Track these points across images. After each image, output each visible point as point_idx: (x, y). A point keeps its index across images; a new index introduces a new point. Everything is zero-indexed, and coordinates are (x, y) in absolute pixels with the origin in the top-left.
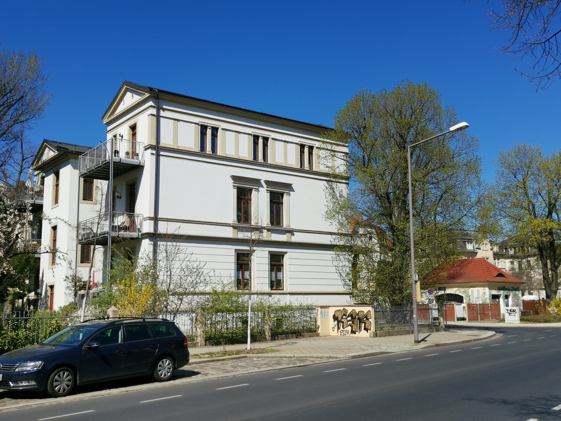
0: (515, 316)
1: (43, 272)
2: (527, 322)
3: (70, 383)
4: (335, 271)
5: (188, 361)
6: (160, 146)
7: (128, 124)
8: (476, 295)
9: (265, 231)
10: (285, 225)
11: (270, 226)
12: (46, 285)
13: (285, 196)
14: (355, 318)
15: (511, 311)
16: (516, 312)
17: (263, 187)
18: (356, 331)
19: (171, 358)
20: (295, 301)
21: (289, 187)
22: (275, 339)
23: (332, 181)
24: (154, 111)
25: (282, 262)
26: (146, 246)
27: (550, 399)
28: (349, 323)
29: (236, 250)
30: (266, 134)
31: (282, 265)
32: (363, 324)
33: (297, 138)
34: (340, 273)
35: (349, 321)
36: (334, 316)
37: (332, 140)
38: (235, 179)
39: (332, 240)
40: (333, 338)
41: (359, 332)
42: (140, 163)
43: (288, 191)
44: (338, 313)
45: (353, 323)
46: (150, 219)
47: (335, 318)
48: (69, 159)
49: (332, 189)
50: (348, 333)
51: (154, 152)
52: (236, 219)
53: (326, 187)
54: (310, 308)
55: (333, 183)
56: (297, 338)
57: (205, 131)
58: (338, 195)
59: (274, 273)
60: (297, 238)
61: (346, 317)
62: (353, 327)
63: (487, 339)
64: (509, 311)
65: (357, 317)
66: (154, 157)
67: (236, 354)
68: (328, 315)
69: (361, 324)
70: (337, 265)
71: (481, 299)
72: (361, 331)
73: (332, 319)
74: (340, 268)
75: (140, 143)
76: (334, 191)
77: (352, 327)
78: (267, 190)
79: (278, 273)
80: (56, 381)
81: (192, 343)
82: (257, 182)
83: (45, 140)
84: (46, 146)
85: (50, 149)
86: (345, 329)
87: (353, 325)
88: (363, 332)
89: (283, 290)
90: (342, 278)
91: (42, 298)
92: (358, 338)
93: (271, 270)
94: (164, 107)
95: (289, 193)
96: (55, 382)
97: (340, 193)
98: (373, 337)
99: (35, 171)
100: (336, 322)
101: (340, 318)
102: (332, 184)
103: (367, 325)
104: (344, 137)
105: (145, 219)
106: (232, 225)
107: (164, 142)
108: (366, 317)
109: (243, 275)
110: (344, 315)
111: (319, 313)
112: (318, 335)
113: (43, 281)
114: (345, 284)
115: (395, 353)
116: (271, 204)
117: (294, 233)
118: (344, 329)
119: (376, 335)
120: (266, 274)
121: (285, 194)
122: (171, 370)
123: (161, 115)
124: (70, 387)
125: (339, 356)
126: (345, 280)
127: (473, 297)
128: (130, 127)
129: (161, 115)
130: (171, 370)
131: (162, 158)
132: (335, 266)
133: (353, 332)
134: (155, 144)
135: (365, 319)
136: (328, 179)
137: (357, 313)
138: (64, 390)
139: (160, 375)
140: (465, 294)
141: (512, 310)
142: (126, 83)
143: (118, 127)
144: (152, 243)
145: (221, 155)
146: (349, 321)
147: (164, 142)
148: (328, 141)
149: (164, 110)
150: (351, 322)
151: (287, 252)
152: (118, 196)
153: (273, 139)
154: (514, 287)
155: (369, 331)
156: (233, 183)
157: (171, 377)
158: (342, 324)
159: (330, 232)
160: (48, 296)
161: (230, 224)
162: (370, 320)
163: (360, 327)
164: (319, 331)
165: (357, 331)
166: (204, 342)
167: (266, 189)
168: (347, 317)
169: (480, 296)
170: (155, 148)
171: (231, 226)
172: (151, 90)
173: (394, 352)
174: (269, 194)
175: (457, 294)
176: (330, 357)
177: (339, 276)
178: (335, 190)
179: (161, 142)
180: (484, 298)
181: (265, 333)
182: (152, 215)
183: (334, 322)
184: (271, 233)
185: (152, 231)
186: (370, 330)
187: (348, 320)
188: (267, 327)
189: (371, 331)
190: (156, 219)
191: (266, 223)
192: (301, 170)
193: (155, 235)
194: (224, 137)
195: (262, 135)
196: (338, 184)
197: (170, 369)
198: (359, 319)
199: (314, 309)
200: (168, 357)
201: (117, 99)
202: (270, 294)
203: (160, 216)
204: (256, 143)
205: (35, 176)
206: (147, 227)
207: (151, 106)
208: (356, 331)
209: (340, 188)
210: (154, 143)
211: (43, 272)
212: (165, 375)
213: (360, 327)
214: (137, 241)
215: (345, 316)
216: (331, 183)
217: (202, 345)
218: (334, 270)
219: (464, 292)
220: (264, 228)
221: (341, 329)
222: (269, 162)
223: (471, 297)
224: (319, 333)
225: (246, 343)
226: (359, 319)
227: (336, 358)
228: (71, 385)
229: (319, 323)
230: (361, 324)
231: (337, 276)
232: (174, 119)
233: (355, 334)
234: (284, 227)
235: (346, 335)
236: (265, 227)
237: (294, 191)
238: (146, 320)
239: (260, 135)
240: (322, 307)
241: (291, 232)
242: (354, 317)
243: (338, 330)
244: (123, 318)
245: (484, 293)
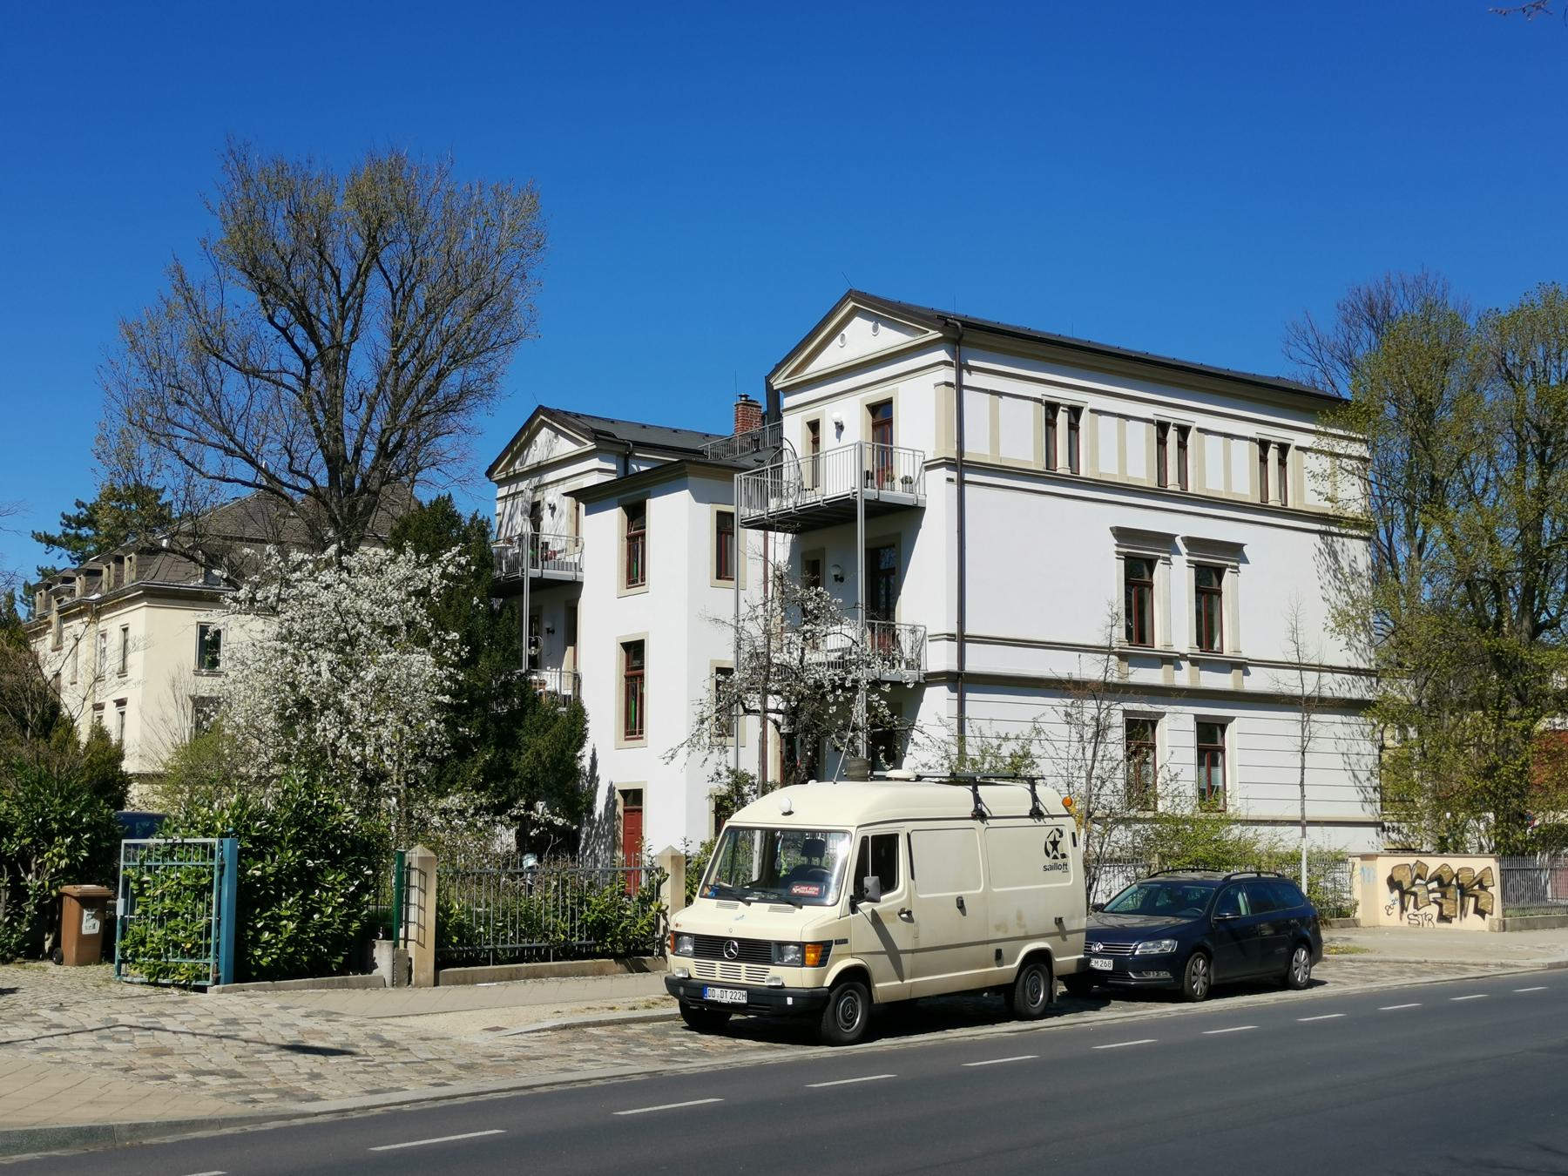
1: (594, 754)
4: (1342, 765)
7: (861, 399)
9: (1185, 664)
11: (1198, 651)
12: (611, 790)
13: (1227, 575)
14: (1450, 884)
17: (1178, 553)
21: (1235, 551)
24: (949, 375)
25: (1151, 738)
26: (936, 704)
28: (1432, 896)
29: (1197, 717)
32: (1472, 900)
33: (1251, 425)
35: (1433, 891)
37: (1359, 433)
38: (1122, 534)
39: (1335, 686)
40: (1393, 931)
45: (1444, 896)
46: (950, 637)
47: (1393, 883)
48: (685, 475)
49: (1334, 554)
51: (954, 475)
55: (1335, 538)
58: (1347, 569)
59: (1204, 770)
60: (1257, 682)
61: (1424, 882)
62: (1444, 907)
65: (1454, 882)
66: (954, 488)
67: (647, 1007)
69: (1467, 898)
70: (1346, 751)
72: (1465, 916)
73: (1383, 887)
74: (1354, 758)
75: (917, 453)
77: (1440, 905)
79: (1213, 770)
82: (1165, 541)
83: (540, 407)
84: (543, 424)
85: (558, 432)
86: (1422, 911)
87: (1444, 901)
90: (1358, 784)
91: (594, 820)
93: (1200, 763)
94: (971, 363)
97: (1350, 565)
98: (1499, 931)
100: (1397, 893)
101: (1406, 885)
103: (1482, 901)
105: (935, 638)
106: (1117, 650)
107: (977, 449)
108: (1480, 883)
110: (1419, 876)
111: (1357, 872)
112: (1356, 923)
113: (594, 779)
114: (1365, 800)
116: (1199, 595)
119: (1504, 927)
121: (1228, 570)
128: (868, 406)
133: (1443, 918)
134: (954, 456)
135: (1476, 887)
136: (1323, 528)
142: (851, 295)
143: (826, 401)
144: (955, 696)
145: (1088, 476)
146: (1433, 891)
148: (1341, 432)
149: (970, 369)
151: (1234, 718)
152: (836, 576)
153: (1200, 430)
155: (1487, 915)
156: (1117, 545)
158: (1413, 898)
159: (1331, 667)
160: (619, 817)
162: (1490, 889)
164: (1358, 915)
165: (1456, 917)
167: (1187, 557)
168: (1428, 883)
176: (1502, 965)
177: (1352, 779)
178: (1340, 558)
182: (954, 630)
185: (953, 666)
186: (1491, 914)
192: (1262, 508)
194: (1094, 429)
195: (1069, 403)
196: (1345, 540)
198: (1460, 886)
199: (1344, 861)
201: (821, 331)
205: (498, 499)
206: (940, 658)
207: (945, 363)
209: (1352, 553)
211: (594, 754)
215: (1422, 879)
216: (1330, 538)
218: (1338, 762)
220: (1184, 657)
221: (1411, 909)
226: (1460, 886)
229: (1357, 895)
230: (1467, 898)
231: (1345, 778)
232: (993, 393)
233: (1451, 922)
235: (1425, 925)
236: (1185, 655)
238: (1263, 875)
240: (1364, 857)
241: (1242, 666)
242: (1446, 882)
243: (1402, 912)
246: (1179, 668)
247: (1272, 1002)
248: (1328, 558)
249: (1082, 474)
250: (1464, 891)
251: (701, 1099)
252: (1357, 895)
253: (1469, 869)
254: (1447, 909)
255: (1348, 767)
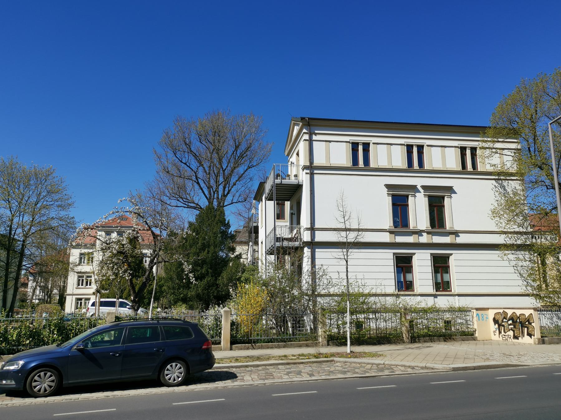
3: (53, 384)
4: (513, 271)
6: (314, 165)
9: (425, 234)
10: (448, 226)
11: (431, 229)
17: (419, 192)
18: (519, 337)
19: (183, 361)
20: (458, 302)
21: (450, 190)
22: (415, 342)
23: (500, 179)
26: (307, 252)
29: (394, 254)
30: (420, 142)
31: (449, 267)
32: (526, 329)
34: (520, 273)
35: (510, 325)
36: (494, 319)
38: (389, 187)
40: (498, 343)
41: (522, 338)
42: (299, 182)
44: (498, 316)
45: (515, 327)
47: (496, 321)
49: (503, 187)
50: (510, 338)
51: (308, 171)
52: (392, 224)
53: (495, 186)
54: (463, 310)
55: (503, 181)
56: (445, 341)
57: (464, 152)
59: (439, 275)
60: (463, 239)
61: (506, 321)
66: (308, 176)
68: (487, 318)
72: (524, 336)
73: (492, 323)
76: (505, 189)
77: (514, 331)
78: (424, 195)
80: (35, 381)
81: (312, 343)
82: (414, 188)
86: (507, 334)
87: (515, 329)
88: (527, 337)
89: (451, 291)
92: (519, 344)
94: (316, 132)
96: (34, 382)
98: (539, 344)
101: (500, 322)
102: (502, 182)
104: (513, 133)
107: (317, 162)
108: (528, 321)
109: (405, 277)
110: (505, 318)
111: (475, 315)
112: (475, 339)
115: (530, 367)
117: (422, 233)
118: (505, 333)
119: (542, 341)
120: (430, 276)
121: (446, 197)
122: (183, 374)
123: (314, 139)
124: (53, 388)
125: (436, 366)
126: (527, 281)
129: (313, 139)
130: (183, 374)
131: (316, 176)
132: (514, 266)
135: (527, 323)
136: (497, 177)
137: (518, 316)
138: (45, 390)
139: (167, 379)
145: (373, 167)
146: (510, 325)
147: (317, 162)
149: (316, 134)
150: (512, 326)
153: (428, 146)
155: (532, 336)
156: (387, 191)
157: (181, 382)
158: (503, 327)
161: (387, 230)
162: (533, 324)
163: (522, 332)
164: (477, 335)
165: (520, 337)
166: (326, 342)
167: (424, 193)
170: (309, 168)
171: (388, 231)
172: (303, 119)
173: (530, 365)
174: (427, 199)
176: (426, 368)
177: (519, 276)
178: (506, 188)
179: (315, 162)
181: (403, 336)
182: (309, 226)
183: (495, 325)
184: (432, 236)
185: (309, 240)
186: (534, 336)
187: (509, 323)
188: (404, 329)
189: (536, 337)
190: (312, 229)
191: (426, 227)
193: (312, 243)
195: (362, 142)
197: (181, 373)
198: (521, 322)
199: (470, 311)
200: (179, 361)
201: (291, 131)
203: (317, 226)
204: (463, 155)
206: (306, 237)
208: (519, 337)
210: (308, 164)
212: (174, 380)
213: (522, 332)
214: (298, 250)
215: (506, 319)
217: (324, 345)
218: (512, 270)
220: (423, 231)
221: (503, 333)
222: (479, 169)
224: (477, 337)
225: (346, 345)
226: (521, 322)
227: (433, 369)
228: (54, 385)
230: (524, 328)
231: (516, 276)
233: (518, 339)
234: (447, 229)
239: (414, 144)
240: (477, 309)
241: (456, 233)
242: (515, 320)
243: (499, 334)
246: (422, 235)
247: (160, 393)
248: (500, 188)
249: (479, 170)
250: (523, 325)
251: (99, 410)
252: (475, 326)
253: (523, 314)
254: (516, 333)
255: (516, 272)
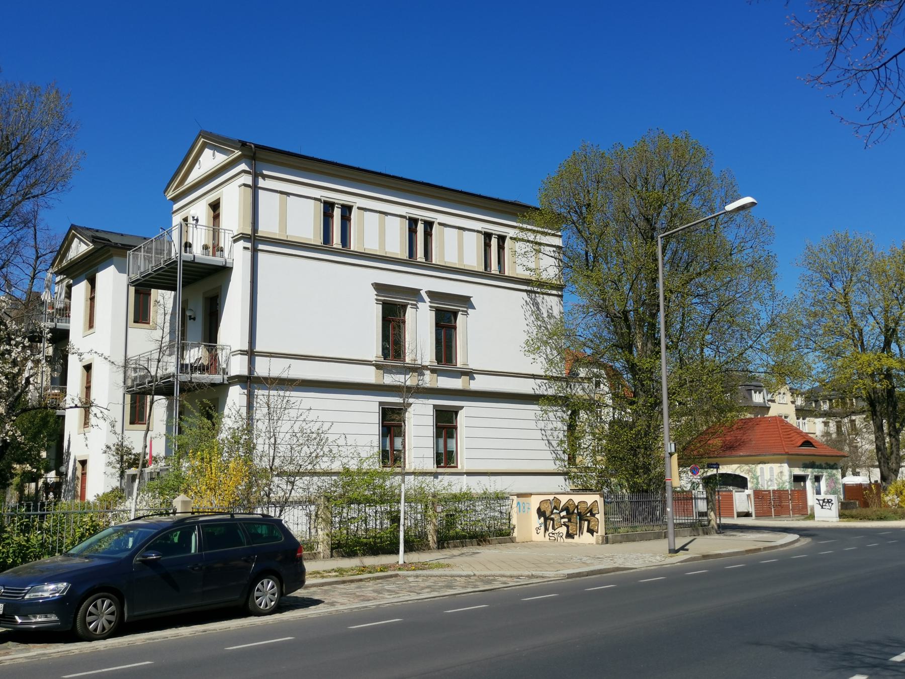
0: (830, 509)
1: (69, 438)
2: (850, 519)
3: (113, 618)
4: (540, 437)
5: (303, 582)
6: (258, 235)
7: (207, 201)
8: (767, 476)
9: (428, 373)
10: (460, 362)
11: (436, 364)
12: (75, 460)
13: (460, 317)
14: (573, 512)
15: (824, 502)
16: (832, 504)
17: (424, 301)
18: (574, 534)
19: (276, 577)
20: (477, 486)
21: (466, 301)
22: (443, 548)
23: (535, 292)
24: (248, 180)
25: (454, 422)
26: (236, 396)
27: (888, 644)
28: (563, 520)
29: (381, 403)
30: (429, 216)
31: (456, 428)
32: (586, 523)
33: (479, 223)
34: (548, 440)
35: (563, 517)
36: (539, 510)
37: (535, 226)
38: (380, 288)
39: (536, 387)
40: (538, 545)
41: (579, 536)
42: (226, 262)
43: (464, 307)
44: (545, 505)
45: (570, 521)
46: (243, 353)
47: (541, 513)
48: (111, 256)
49: (536, 304)
50: (561, 537)
51: (249, 245)
52: (380, 353)
53: (526, 301)
54: (500, 497)
55: (537, 295)
56: (479, 545)
57: (330, 211)
58: (545, 315)
59: (441, 441)
60: (480, 384)
61: (558, 512)
62: (570, 528)
63: (785, 546)
64: (821, 502)
65: (576, 511)
66: (249, 254)
67: (381, 571)
68: (529, 508)
69: (583, 522)
70: (543, 428)
71: (775, 482)
72: (582, 534)
73: (535, 515)
74: (549, 433)
75: (226, 231)
76: (538, 309)
77: (568, 527)
78: (431, 307)
79: (449, 440)
80: (91, 614)
81: (309, 554)
82: (414, 293)
83: (72, 225)
84: (74, 236)
85: (81, 240)
86: (557, 531)
87: (570, 524)
88: (586, 536)
89: (457, 467)
90: (552, 448)
91: (67, 480)
92: (577, 545)
93: (438, 435)
94: (265, 172)
95: (466, 312)
96: (89, 616)
97: (548, 312)
98: (602, 543)
99: (57, 277)
100: (542, 519)
101: (548, 514)
102: (535, 296)
103: (592, 523)
104: (554, 222)
105: (234, 353)
106: (374, 362)
107: (264, 229)
108: (591, 511)
109: (392, 443)
110: (555, 508)
111: (515, 505)
112: (513, 540)
113: (69, 454)
114: (557, 459)
115: (638, 570)
116: (437, 328)
117: (474, 375)
118: (555, 530)
119: (606, 540)
120: (430, 442)
121: (460, 313)
122: (276, 596)
123: (260, 185)
124: (113, 624)
125: (546, 574)
126: (556, 452)
127: (763, 479)
128: (209, 205)
129: (259, 186)
130: (276, 596)
131: (261, 256)
132: (541, 430)
133: (569, 535)
134: (250, 232)
135: (589, 515)
136: (529, 288)
137: (576, 504)
138: (104, 629)
139: (258, 605)
140: (750, 473)
141: (826, 501)
142: (203, 134)
143: (190, 205)
144: (246, 391)
145: (356, 250)
146: (563, 517)
147: (264, 229)
148: (529, 227)
149: (264, 177)
150: (566, 520)
151: (463, 407)
152: (190, 316)
153: (440, 224)
154: (828, 462)
155: (595, 533)
156: (376, 295)
157: (275, 608)
158: (552, 522)
159: (533, 375)
160: (78, 478)
161: (372, 362)
162: (597, 516)
163: (580, 527)
164: (515, 534)
165: (576, 534)
166: (328, 552)
167: (429, 304)
168: (560, 512)
169: (775, 477)
170: (250, 238)
171: (373, 365)
172: (243, 145)
173: (636, 568)
174: (434, 313)
175: (737, 474)
176: (533, 576)
177: (548, 445)
178: (540, 307)
179: (260, 229)
180: (781, 481)
181: (427, 538)
182: (246, 347)
183: (539, 519)
184: (438, 376)
185: (245, 372)
186: (597, 532)
187: (562, 516)
188: (430, 528)
189: (599, 534)
190: (251, 353)
191: (429, 360)
192: (486, 274)
193: (250, 379)
194: (361, 221)
195: (423, 218)
196: (545, 296)
197: (274, 594)
198: (579, 514)
199: (507, 498)
200: (271, 576)
201: (188, 160)
202: (435, 475)
203: (258, 348)
204: (412, 231)
205: (56, 284)
206: (238, 366)
207: (244, 171)
208: (574, 534)
209: (549, 304)
210: (249, 231)
211: (69, 438)
212: (266, 606)
213: (580, 527)
214: (220, 389)
215: (557, 509)
216: (534, 295)
217: (326, 556)
218: (538, 435)
219: (749, 471)
220: (426, 368)
221: (551, 530)
222: (435, 261)
223: (760, 479)
224: (515, 537)
225: (397, 552)
226: (579, 514)
227: (543, 577)
228: (114, 620)
229: (514, 521)
230: (583, 522)
231: (543, 445)
232: (281, 193)
233: (573, 538)
234: (458, 366)
235: (559, 541)
236: (427, 366)
237: (475, 308)
238: (236, 516)
239: (420, 218)
240: (519, 495)
241: (470, 374)
242: (571, 511)
243: (545, 532)
244: (198, 512)
245: (781, 472)
